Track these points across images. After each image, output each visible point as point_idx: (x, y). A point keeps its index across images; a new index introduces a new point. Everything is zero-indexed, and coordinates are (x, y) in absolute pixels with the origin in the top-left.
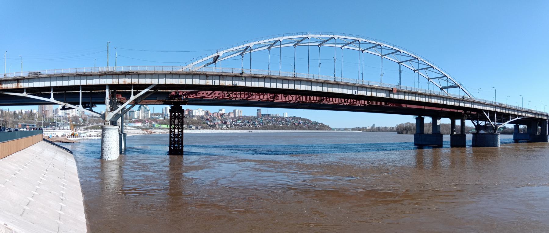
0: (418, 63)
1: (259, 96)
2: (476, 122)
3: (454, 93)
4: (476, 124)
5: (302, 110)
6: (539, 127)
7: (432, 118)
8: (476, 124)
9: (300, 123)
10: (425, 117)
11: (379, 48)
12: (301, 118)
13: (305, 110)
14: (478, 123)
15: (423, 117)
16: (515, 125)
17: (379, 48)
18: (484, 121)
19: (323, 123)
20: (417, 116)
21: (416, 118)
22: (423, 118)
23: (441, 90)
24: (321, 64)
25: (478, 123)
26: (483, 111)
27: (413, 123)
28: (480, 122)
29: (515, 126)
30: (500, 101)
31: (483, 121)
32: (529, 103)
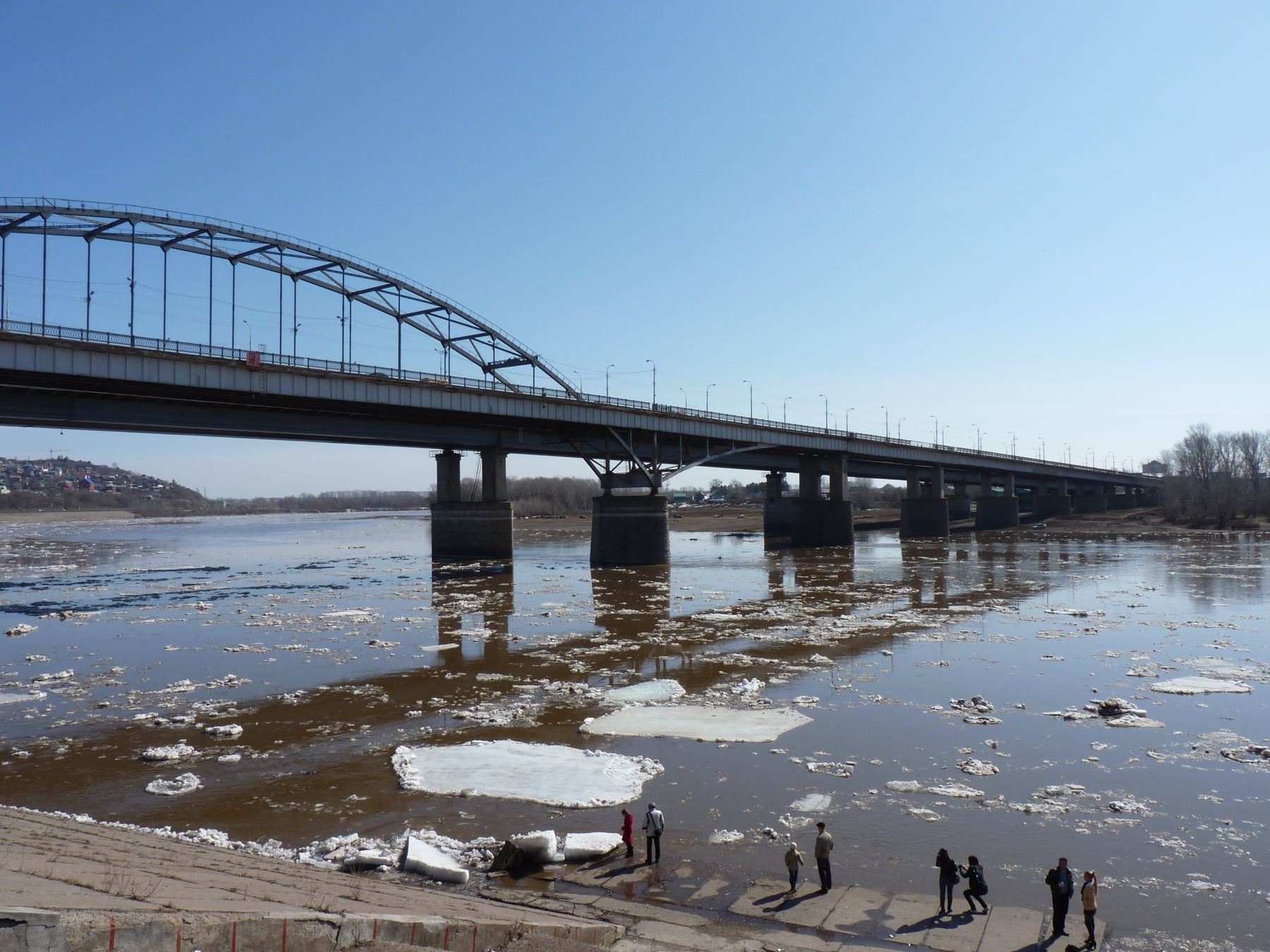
0: (399, 295)
1: (166, 339)
2: (600, 463)
3: (520, 377)
4: (603, 471)
5: (58, 431)
6: (778, 473)
7: (482, 455)
8: (603, 471)
9: (85, 484)
10: (464, 452)
11: (275, 253)
12: (95, 463)
13: (67, 431)
14: (607, 468)
15: (456, 452)
16: (769, 472)
17: (275, 253)
18: (626, 460)
19: (176, 481)
20: (440, 451)
21: (437, 457)
22: (459, 456)
23: (485, 373)
24: (93, 293)
25: (607, 468)
26: (613, 431)
27: (588, 478)
28: (613, 463)
29: (767, 476)
30: (671, 398)
31: (622, 458)
32: (788, 402)
